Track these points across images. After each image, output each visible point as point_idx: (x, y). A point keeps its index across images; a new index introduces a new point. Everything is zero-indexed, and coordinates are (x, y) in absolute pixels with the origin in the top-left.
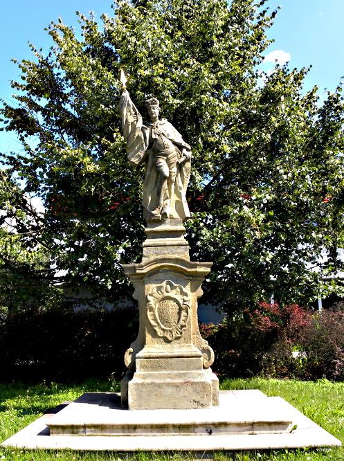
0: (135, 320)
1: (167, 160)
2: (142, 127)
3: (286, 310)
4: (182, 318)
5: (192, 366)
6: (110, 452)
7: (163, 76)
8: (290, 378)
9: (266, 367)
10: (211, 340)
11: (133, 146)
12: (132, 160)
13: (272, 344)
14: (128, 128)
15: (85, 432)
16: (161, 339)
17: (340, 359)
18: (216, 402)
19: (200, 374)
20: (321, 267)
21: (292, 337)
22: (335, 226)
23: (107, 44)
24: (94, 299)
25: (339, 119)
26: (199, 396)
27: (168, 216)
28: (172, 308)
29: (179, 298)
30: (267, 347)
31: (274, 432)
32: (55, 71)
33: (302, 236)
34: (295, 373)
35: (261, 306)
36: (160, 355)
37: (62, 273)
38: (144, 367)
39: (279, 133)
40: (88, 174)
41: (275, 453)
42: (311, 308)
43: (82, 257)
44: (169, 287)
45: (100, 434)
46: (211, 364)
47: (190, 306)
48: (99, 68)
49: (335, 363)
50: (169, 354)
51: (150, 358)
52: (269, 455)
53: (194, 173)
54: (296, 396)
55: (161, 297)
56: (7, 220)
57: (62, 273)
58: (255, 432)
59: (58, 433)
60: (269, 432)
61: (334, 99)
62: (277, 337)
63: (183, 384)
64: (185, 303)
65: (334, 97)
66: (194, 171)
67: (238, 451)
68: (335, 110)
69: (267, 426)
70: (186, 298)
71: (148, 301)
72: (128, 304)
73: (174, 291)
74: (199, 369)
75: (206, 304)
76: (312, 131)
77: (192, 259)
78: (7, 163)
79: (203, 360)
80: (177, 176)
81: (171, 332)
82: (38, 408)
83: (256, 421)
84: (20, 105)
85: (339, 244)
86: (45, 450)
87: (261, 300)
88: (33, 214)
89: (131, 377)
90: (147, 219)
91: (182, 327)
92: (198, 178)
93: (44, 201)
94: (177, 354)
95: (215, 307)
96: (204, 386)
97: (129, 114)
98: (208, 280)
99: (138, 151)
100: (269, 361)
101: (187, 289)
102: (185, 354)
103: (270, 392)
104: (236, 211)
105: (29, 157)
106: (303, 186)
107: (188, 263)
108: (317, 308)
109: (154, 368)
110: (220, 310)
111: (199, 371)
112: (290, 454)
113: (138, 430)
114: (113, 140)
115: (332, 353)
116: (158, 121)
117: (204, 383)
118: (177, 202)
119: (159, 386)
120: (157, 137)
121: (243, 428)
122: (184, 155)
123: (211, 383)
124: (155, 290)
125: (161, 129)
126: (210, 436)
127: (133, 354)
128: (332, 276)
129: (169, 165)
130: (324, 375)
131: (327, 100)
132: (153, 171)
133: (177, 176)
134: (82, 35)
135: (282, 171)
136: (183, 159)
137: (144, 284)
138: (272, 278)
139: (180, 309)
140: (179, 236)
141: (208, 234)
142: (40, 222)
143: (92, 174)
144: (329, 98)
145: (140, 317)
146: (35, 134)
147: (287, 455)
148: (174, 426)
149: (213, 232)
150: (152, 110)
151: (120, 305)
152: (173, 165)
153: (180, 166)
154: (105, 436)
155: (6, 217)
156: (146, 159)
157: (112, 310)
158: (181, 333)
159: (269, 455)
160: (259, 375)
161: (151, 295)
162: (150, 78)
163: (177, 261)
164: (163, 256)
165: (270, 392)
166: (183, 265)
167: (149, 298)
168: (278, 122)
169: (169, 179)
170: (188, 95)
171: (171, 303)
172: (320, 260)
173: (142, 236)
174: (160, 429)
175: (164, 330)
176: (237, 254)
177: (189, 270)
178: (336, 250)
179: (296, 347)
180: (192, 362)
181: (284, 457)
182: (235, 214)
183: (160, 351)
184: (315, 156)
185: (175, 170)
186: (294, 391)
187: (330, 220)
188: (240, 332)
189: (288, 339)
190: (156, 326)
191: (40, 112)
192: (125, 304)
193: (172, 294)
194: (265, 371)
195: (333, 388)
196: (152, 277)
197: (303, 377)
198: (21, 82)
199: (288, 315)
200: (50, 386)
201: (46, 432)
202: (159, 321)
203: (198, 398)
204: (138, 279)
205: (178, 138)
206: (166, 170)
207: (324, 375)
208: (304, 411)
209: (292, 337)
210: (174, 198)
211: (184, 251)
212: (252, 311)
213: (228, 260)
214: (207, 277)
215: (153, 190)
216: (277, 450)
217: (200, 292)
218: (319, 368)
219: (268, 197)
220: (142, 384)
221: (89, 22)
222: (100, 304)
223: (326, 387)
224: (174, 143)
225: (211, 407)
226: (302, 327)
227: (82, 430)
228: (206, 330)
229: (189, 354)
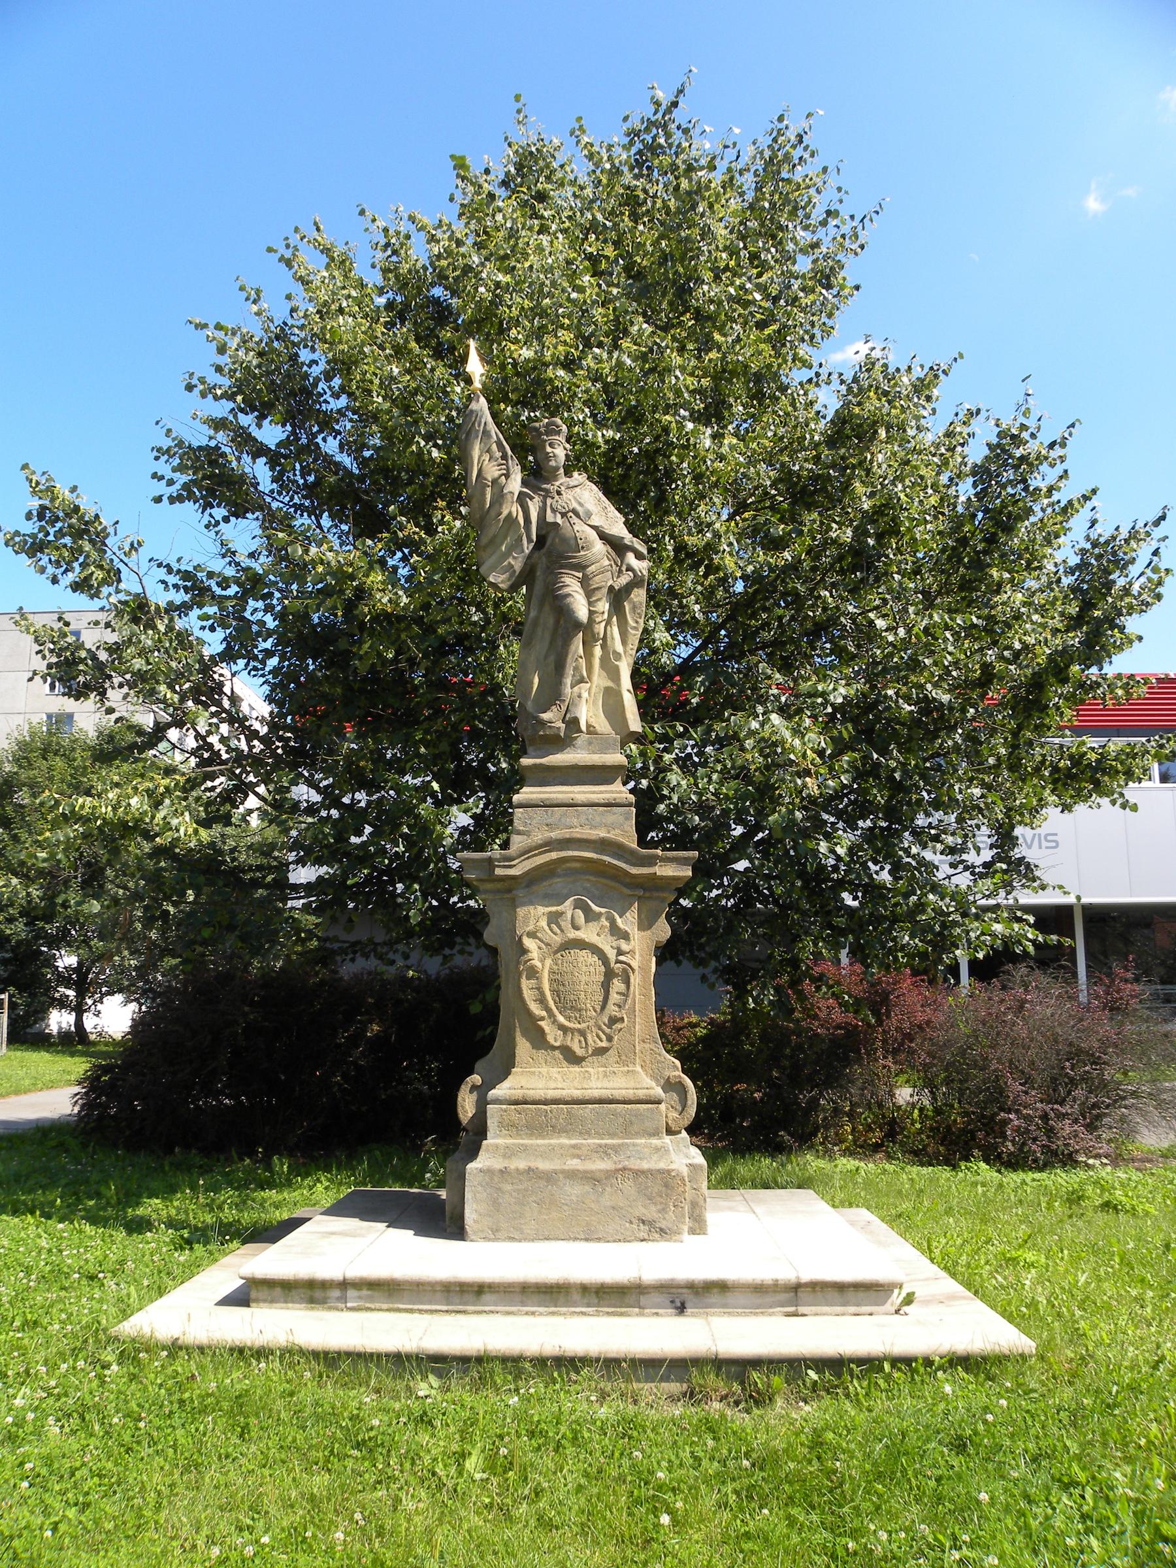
0: (489, 997)
1: (585, 582)
2: (521, 493)
3: (879, 982)
4: (614, 997)
5: (636, 1128)
6: (409, 1357)
7: (569, 364)
8: (890, 1157)
9: (827, 1128)
10: (685, 1056)
11: (494, 542)
12: (491, 579)
13: (845, 1067)
14: (484, 495)
15: (343, 1299)
16: (557, 1053)
17: (1017, 1112)
18: (698, 1226)
19: (657, 1149)
20: (973, 873)
21: (895, 1052)
22: (1014, 766)
23: (437, 292)
24: (390, 944)
25: (1026, 489)
26: (653, 1208)
27: (583, 727)
28: (587, 968)
29: (607, 945)
30: (833, 1079)
31: (852, 1309)
32: (305, 355)
33: (929, 793)
34: (902, 1144)
35: (817, 970)
36: (551, 1094)
37: (303, 875)
38: (510, 1127)
39: (873, 522)
40: (378, 615)
41: (857, 1370)
42: (946, 980)
43: (359, 833)
44: (580, 916)
45: (385, 1306)
46: (687, 1123)
47: (635, 964)
48: (410, 351)
49: (1005, 1122)
50: (577, 1094)
51: (526, 1102)
52: (839, 1375)
53: (651, 623)
54: (906, 1206)
55: (558, 939)
56: (173, 734)
57: (303, 875)
58: (802, 1310)
59: (272, 1301)
60: (839, 1309)
61: (1013, 437)
62: (858, 1051)
63: (610, 1174)
64: (622, 958)
65: (1015, 431)
66: (652, 618)
67: (756, 1363)
68: (1016, 467)
69: (834, 1295)
70: (625, 946)
71: (525, 951)
72: (478, 958)
73: (594, 927)
74: (655, 1134)
75: (679, 963)
76: (957, 522)
77: (642, 842)
78: (176, 586)
79: (667, 1111)
80: (609, 623)
81: (582, 1033)
82: (230, 1224)
83: (806, 1277)
84: (211, 438)
85: (1022, 815)
86: (232, 1350)
87: (818, 955)
88: (237, 720)
89: (473, 1153)
90: (527, 734)
91: (613, 1020)
92: (662, 636)
93: (266, 688)
94: (596, 1093)
95: (701, 970)
96: (667, 1180)
97: (486, 457)
98: (684, 902)
99: (508, 554)
100: (837, 1111)
101: (628, 921)
102: (618, 1094)
103: (840, 1196)
104: (754, 725)
105: (230, 572)
106: (935, 664)
107: (632, 852)
108: (957, 977)
109: (536, 1129)
110: (713, 978)
111: (655, 1141)
112: (896, 1375)
113: (487, 1297)
114: (431, 530)
115: (997, 1096)
116: (563, 479)
117: (669, 1172)
118: (607, 691)
119: (548, 1177)
120: (559, 520)
121: (769, 1299)
122: (629, 569)
123: (685, 1171)
124: (543, 923)
125: (569, 499)
126: (681, 1320)
127: (481, 1091)
128: (1001, 899)
129: (589, 593)
130: (976, 1152)
131: (995, 441)
132: (547, 608)
133: (609, 623)
134: (373, 266)
135: (880, 624)
136: (625, 579)
137: (514, 905)
138: (848, 900)
139: (609, 975)
140: (610, 782)
141: (684, 783)
142: (256, 742)
143: (387, 616)
144: (999, 435)
145: (502, 992)
146: (249, 515)
147: (888, 1378)
148: (585, 1289)
149: (696, 779)
150: (549, 449)
151: (458, 960)
152: (598, 595)
153: (618, 597)
154: (399, 1310)
155: (169, 726)
156: (527, 576)
157: (438, 973)
158: (610, 1039)
159: (839, 1375)
160: (811, 1147)
161: (532, 935)
162: (539, 364)
163: (604, 845)
164: (563, 833)
165: (840, 1196)
166: (619, 857)
167: (528, 943)
168: (872, 495)
169: (587, 629)
170: (634, 416)
171: (585, 956)
172: (971, 857)
173: (517, 779)
174: (548, 1297)
175: (562, 1028)
176: (760, 835)
177: (634, 871)
178: (1013, 828)
179: (902, 1078)
180: (638, 1115)
181: (881, 1382)
182: (752, 733)
183: (553, 1085)
184: (966, 586)
185: (604, 606)
186: (900, 1192)
187: (1003, 751)
188: (764, 1037)
189: (885, 1057)
190: (542, 1019)
191: (262, 460)
192: (465, 960)
193: (589, 933)
194: (825, 1138)
195: (1001, 1186)
196: (535, 888)
197: (921, 1156)
198: (213, 378)
199: (885, 998)
200: (269, 1167)
201: (240, 1299)
202: (551, 1004)
203: (651, 1212)
204: (498, 891)
205: (617, 526)
206: (581, 611)
207: (976, 1152)
208: (931, 1251)
209: (895, 1052)
210: (599, 680)
211: (621, 819)
212: (795, 983)
213: (739, 848)
214: (682, 892)
215: (546, 657)
216: (861, 1361)
217: (663, 930)
218: (963, 1131)
219: (842, 691)
220: (503, 1172)
221: (391, 232)
222: (406, 957)
223: (983, 1185)
224: (603, 536)
225: (686, 1237)
226: (920, 1027)
227: (336, 1293)
228: (678, 1029)
229: (630, 1094)
